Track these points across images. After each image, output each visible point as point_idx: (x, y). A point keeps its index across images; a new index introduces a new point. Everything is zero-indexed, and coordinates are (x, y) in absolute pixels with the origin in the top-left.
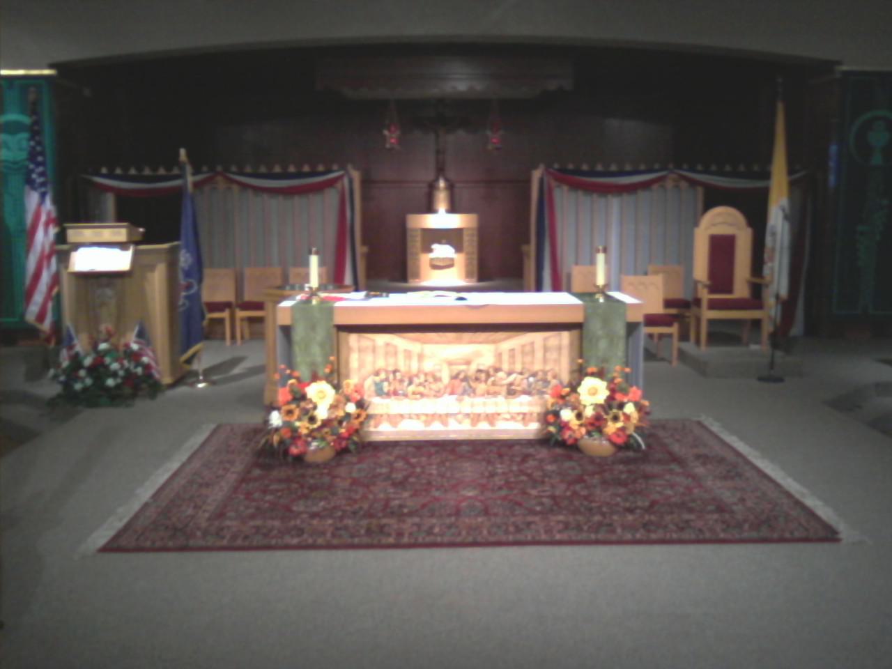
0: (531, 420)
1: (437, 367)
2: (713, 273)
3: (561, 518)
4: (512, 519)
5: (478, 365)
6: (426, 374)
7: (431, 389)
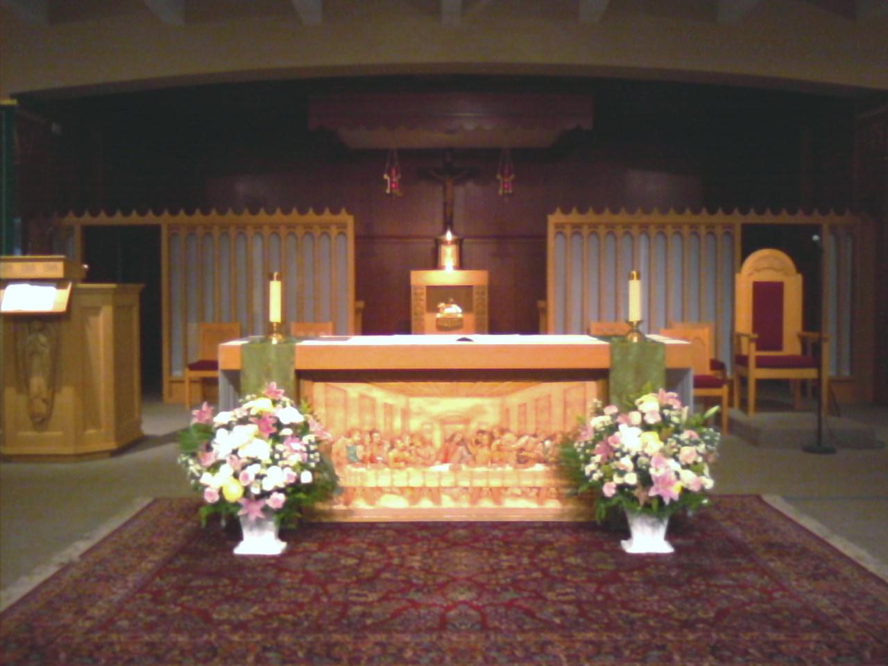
0: (548, 497)
1: (428, 427)
2: (758, 324)
3: (590, 635)
4: (519, 638)
5: (480, 423)
6: (412, 436)
7: (418, 455)
